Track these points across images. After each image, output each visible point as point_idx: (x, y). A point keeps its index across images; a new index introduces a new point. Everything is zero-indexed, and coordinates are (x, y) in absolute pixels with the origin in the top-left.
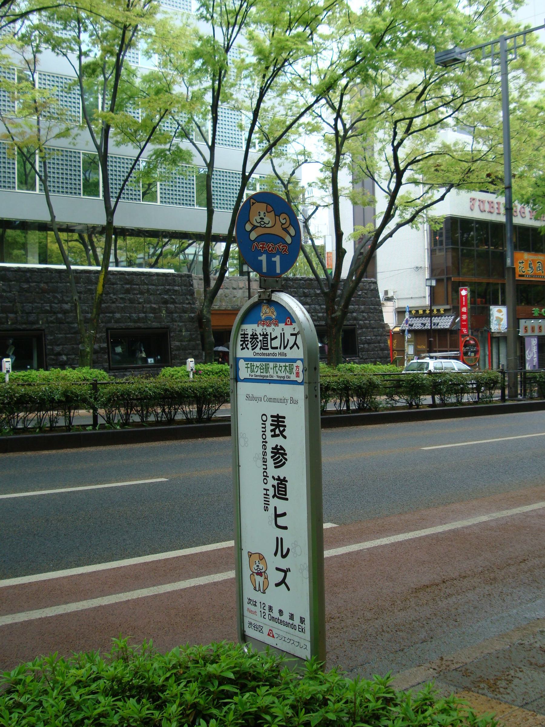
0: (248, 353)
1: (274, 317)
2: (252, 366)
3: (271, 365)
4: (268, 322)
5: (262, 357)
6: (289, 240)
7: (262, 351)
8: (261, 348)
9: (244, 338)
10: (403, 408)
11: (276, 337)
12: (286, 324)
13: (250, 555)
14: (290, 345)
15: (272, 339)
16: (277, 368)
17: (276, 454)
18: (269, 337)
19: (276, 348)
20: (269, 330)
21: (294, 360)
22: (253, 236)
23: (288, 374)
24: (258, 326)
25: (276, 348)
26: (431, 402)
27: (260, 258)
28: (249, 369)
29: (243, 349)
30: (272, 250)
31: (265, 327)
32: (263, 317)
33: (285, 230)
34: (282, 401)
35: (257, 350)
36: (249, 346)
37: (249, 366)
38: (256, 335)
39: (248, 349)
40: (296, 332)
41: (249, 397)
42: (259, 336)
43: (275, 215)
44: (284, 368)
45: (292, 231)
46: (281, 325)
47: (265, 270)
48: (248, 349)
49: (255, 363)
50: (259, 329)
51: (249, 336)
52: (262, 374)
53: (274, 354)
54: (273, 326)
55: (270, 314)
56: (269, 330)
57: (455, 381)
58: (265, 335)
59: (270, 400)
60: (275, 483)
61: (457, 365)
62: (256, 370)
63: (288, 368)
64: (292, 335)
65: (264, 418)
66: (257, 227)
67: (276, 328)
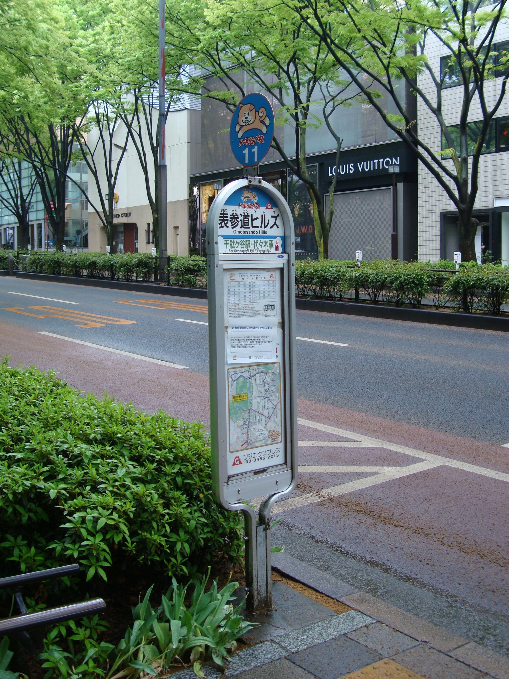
0: (228, 231)
1: (255, 201)
3: (252, 241)
4: (249, 205)
5: (243, 234)
6: (264, 130)
7: (243, 229)
9: (224, 217)
11: (257, 218)
12: (267, 208)
15: (253, 220)
16: (258, 244)
19: (258, 227)
20: (250, 212)
21: (275, 237)
22: (240, 135)
23: (268, 248)
24: (239, 207)
25: (258, 227)
26: (354, 297)
27: (244, 152)
28: (229, 246)
30: (252, 143)
31: (246, 209)
32: (244, 200)
33: (263, 122)
35: (238, 228)
36: (229, 224)
37: (229, 242)
38: (236, 215)
39: (228, 227)
40: (276, 215)
42: (240, 216)
43: (256, 111)
44: (264, 244)
45: (267, 122)
46: (263, 209)
47: (247, 161)
48: (228, 227)
49: (235, 240)
50: (240, 211)
51: (229, 216)
52: (242, 249)
53: (255, 232)
54: (254, 209)
55: (252, 198)
56: (250, 212)
57: (183, 450)
58: (246, 216)
62: (236, 246)
63: (268, 244)
64: (272, 217)
66: (243, 126)
67: (257, 210)
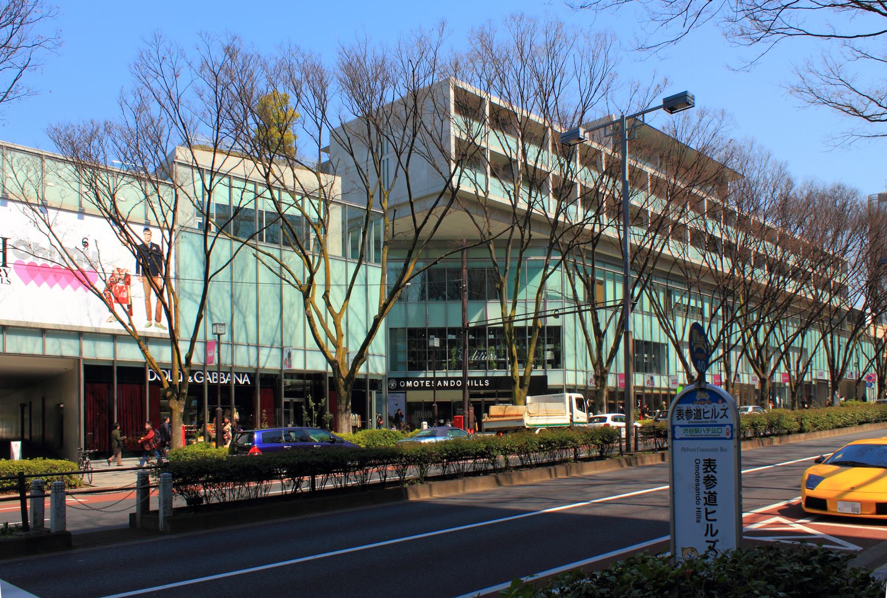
2: (687, 430)
4: (703, 401)
8: (695, 418)
10: (493, 404)
13: (683, 549)
14: (720, 416)
17: (707, 480)
18: (702, 412)
20: (702, 407)
29: (679, 419)
34: (715, 450)
35: (692, 420)
36: (685, 417)
41: (683, 449)
56: (702, 407)
58: (698, 411)
59: (703, 450)
60: (707, 496)
61: (423, 441)
65: (698, 462)
